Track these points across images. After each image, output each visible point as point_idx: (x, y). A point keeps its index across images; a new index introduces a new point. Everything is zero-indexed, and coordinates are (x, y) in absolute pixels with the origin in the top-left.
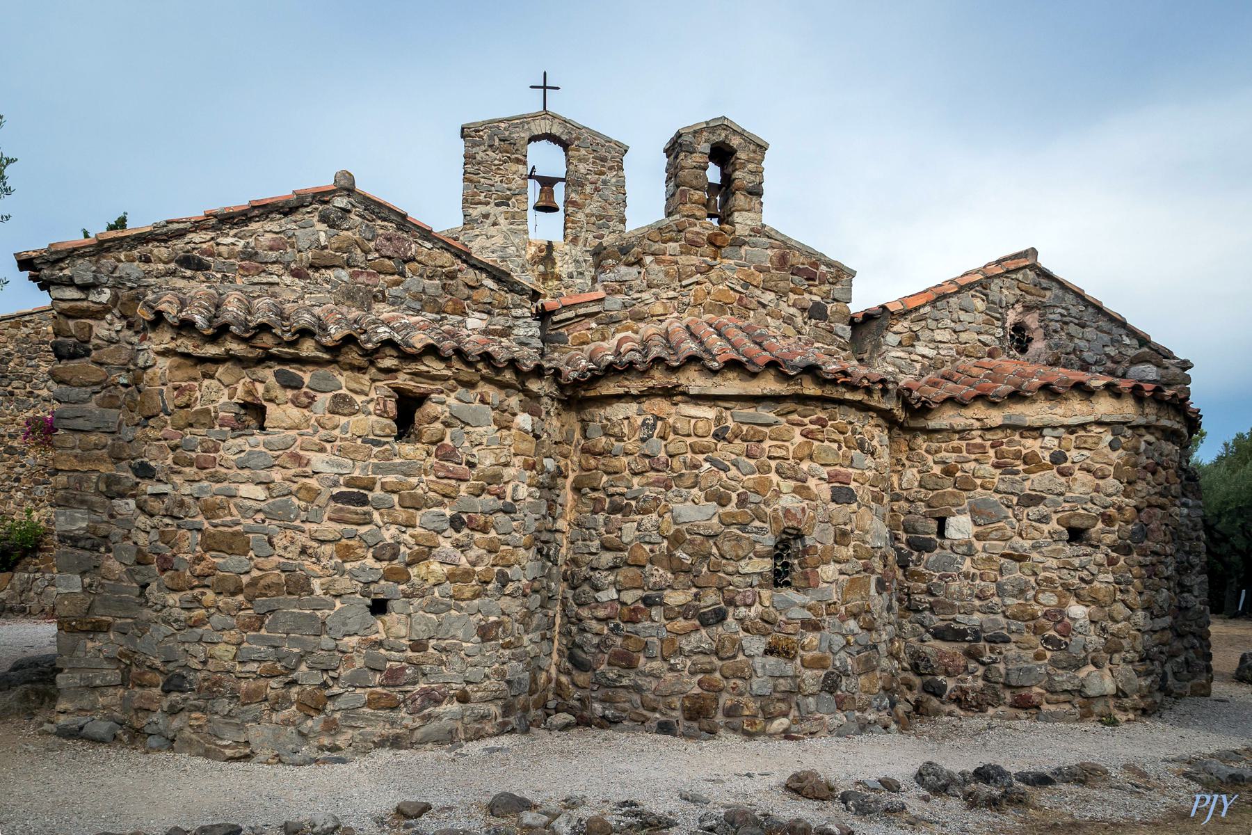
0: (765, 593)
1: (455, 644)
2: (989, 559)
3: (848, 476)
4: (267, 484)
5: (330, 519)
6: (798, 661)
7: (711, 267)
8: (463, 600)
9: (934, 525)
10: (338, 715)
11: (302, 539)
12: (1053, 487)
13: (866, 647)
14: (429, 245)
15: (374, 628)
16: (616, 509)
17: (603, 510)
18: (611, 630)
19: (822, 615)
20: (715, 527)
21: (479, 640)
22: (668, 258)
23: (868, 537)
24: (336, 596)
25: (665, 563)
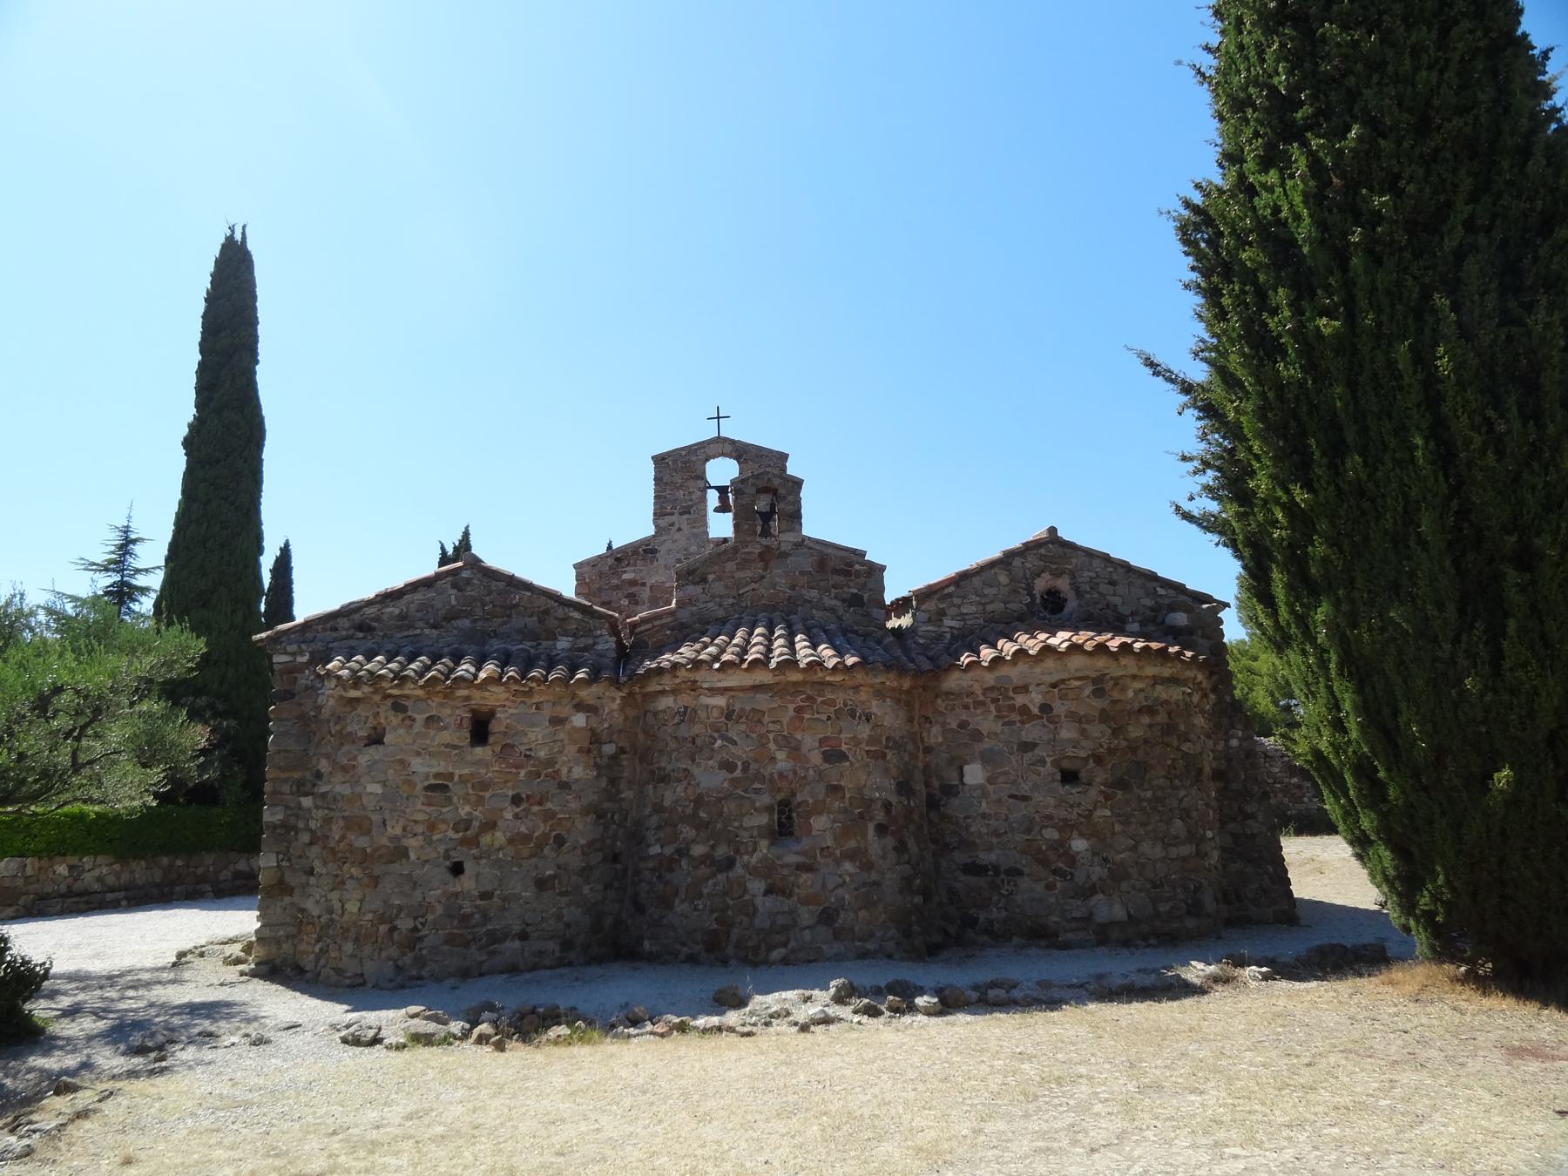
6: (795, 898)
7: (763, 577)
9: (955, 775)
10: (424, 952)
14: (529, 594)
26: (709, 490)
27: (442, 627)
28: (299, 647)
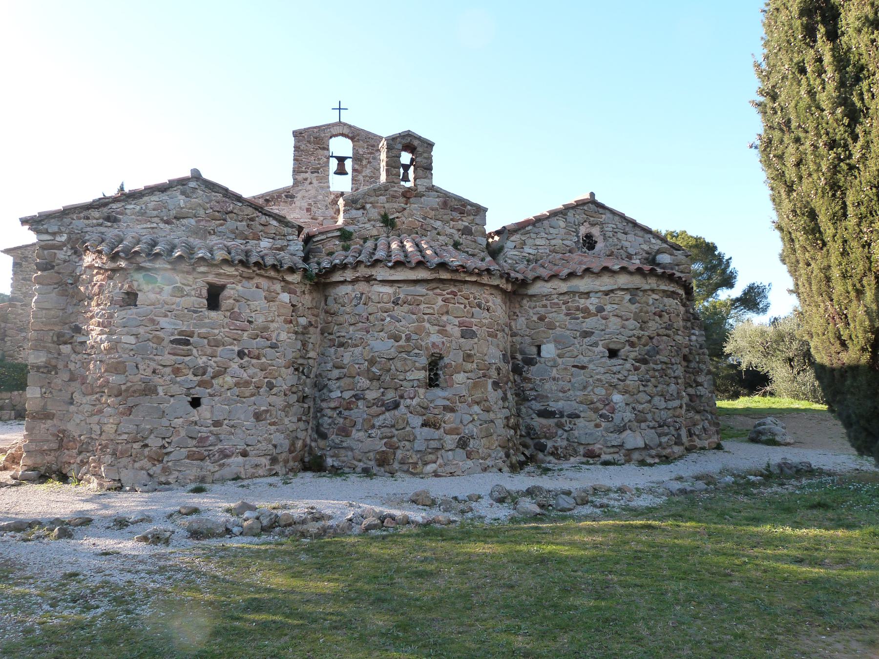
0: (421, 391)
1: (239, 423)
2: (566, 369)
3: (471, 323)
4: (136, 335)
5: (169, 353)
6: (442, 430)
7: (405, 209)
8: (245, 398)
9: (535, 350)
10: (170, 464)
11: (153, 365)
12: (597, 326)
13: (486, 422)
14: (240, 204)
15: (191, 414)
16: (342, 345)
17: (334, 345)
18: (338, 414)
19: (456, 403)
20: (393, 354)
21: (255, 420)
22: (379, 205)
23: (486, 358)
24: (172, 396)
25: (366, 375)
26: (331, 159)
27: (172, 223)
28: (59, 229)
